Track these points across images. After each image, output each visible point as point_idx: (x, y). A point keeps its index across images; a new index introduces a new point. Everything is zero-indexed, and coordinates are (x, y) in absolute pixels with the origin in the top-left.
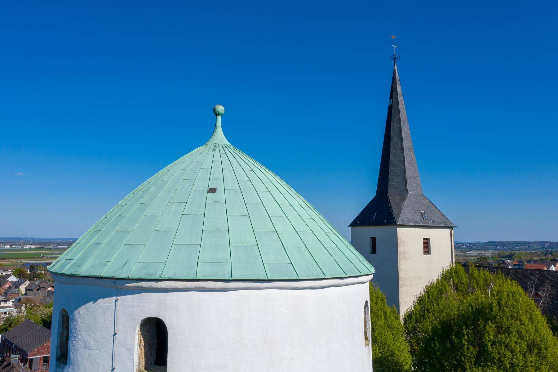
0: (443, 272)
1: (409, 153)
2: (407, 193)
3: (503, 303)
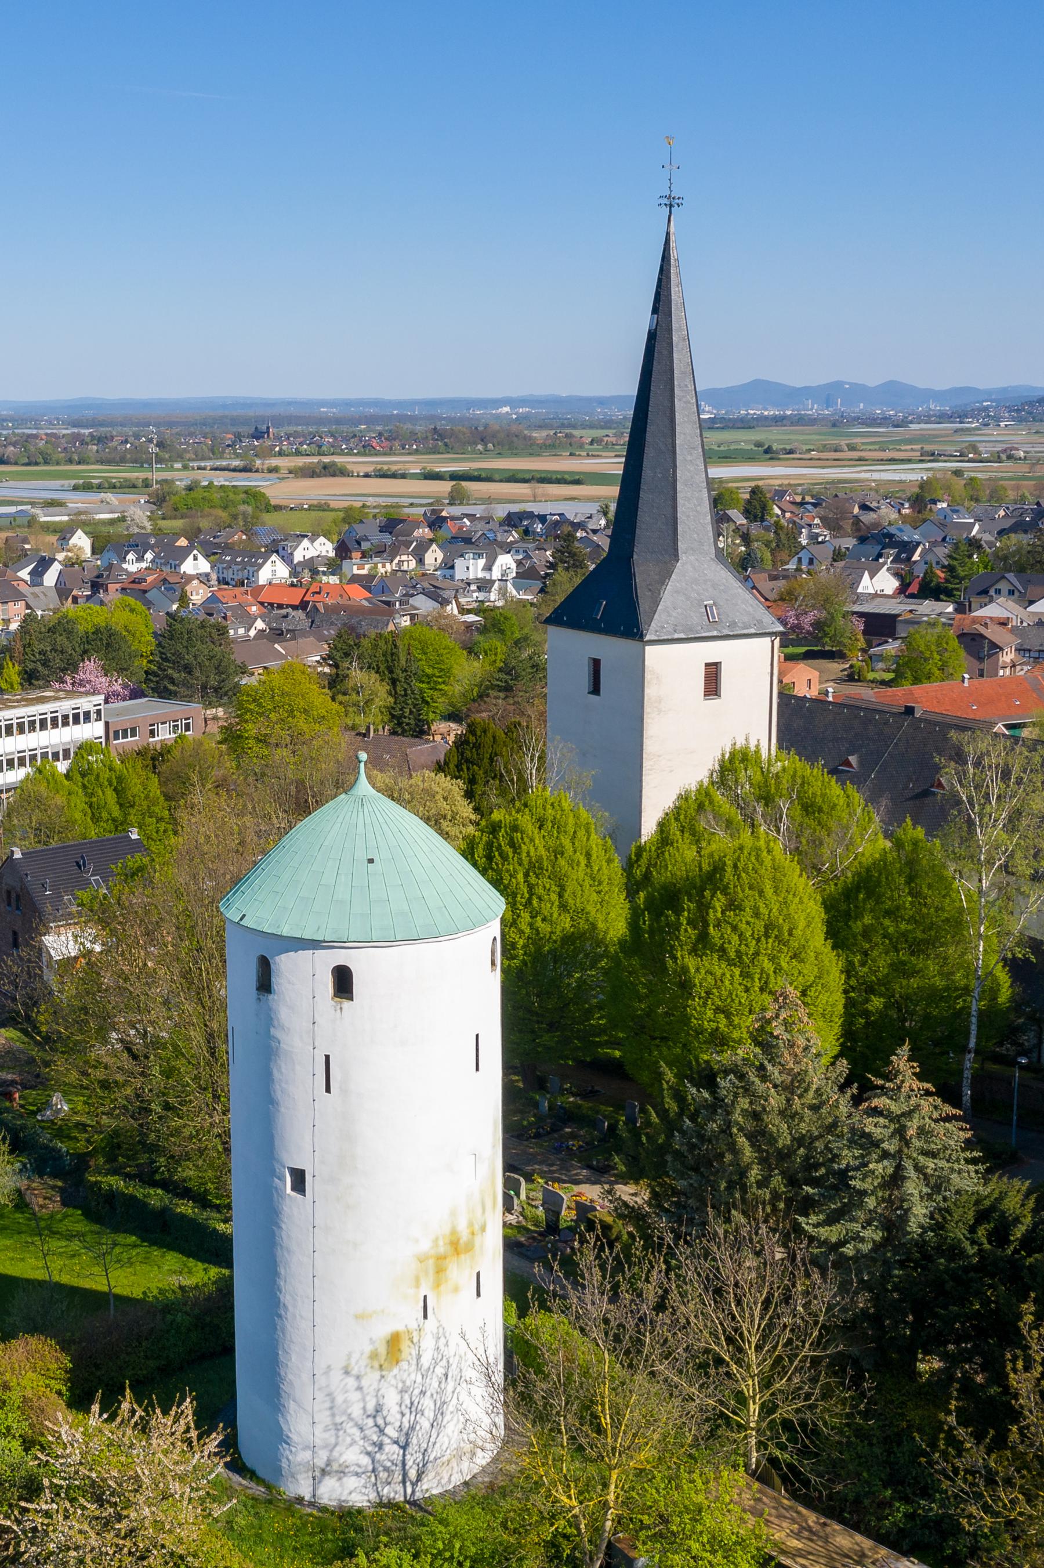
0: (723, 755)
2: (676, 558)
3: (740, 865)
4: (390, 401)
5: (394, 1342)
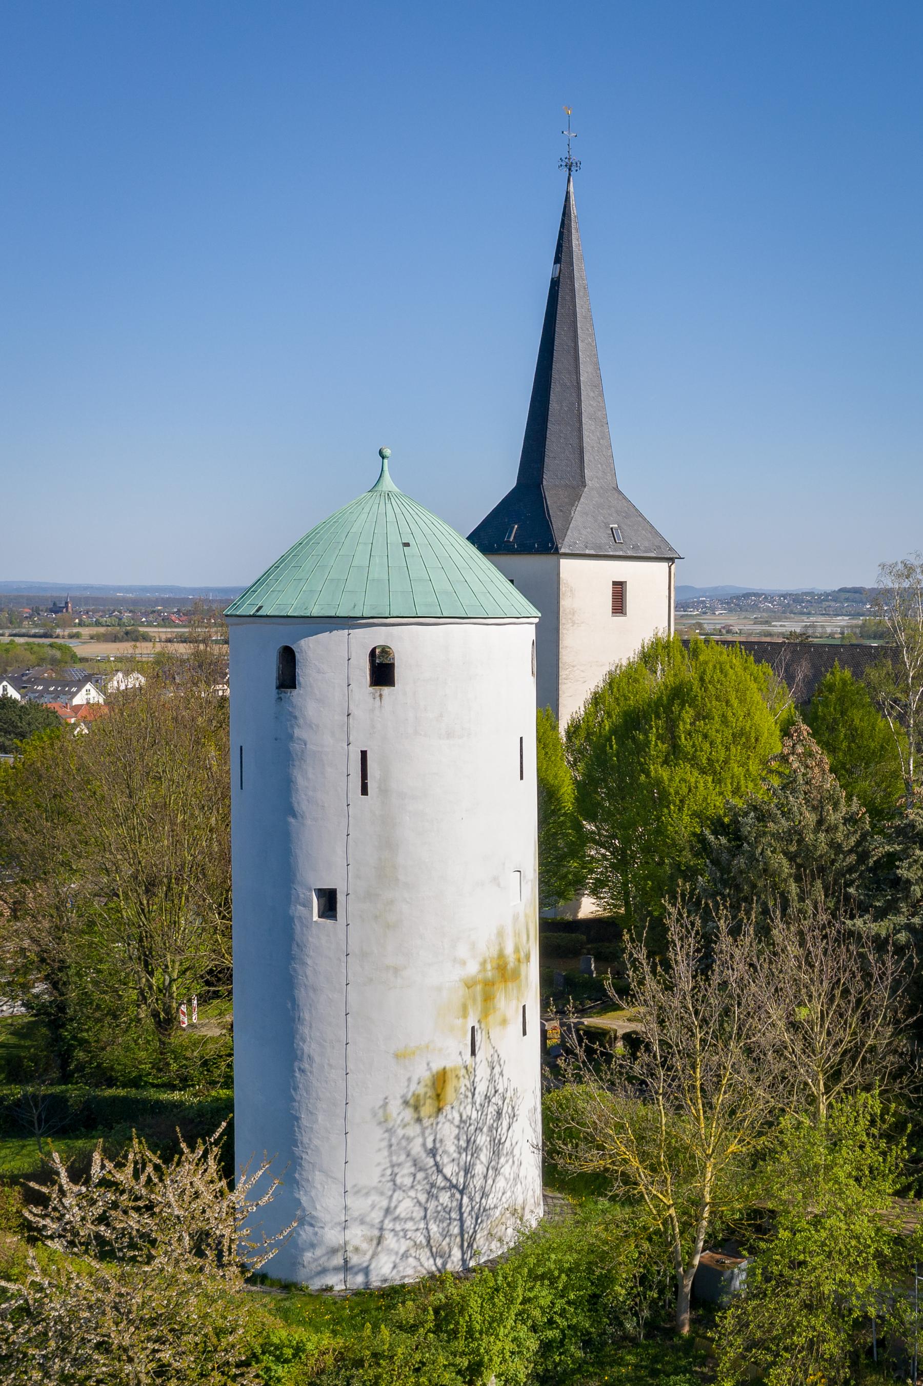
0: (643, 647)
1: (592, 394)
2: (584, 484)
4: (185, 589)
5: (439, 1082)
